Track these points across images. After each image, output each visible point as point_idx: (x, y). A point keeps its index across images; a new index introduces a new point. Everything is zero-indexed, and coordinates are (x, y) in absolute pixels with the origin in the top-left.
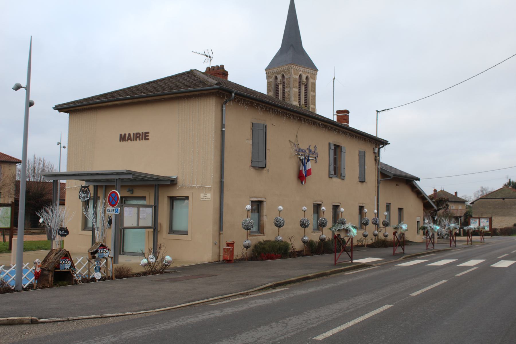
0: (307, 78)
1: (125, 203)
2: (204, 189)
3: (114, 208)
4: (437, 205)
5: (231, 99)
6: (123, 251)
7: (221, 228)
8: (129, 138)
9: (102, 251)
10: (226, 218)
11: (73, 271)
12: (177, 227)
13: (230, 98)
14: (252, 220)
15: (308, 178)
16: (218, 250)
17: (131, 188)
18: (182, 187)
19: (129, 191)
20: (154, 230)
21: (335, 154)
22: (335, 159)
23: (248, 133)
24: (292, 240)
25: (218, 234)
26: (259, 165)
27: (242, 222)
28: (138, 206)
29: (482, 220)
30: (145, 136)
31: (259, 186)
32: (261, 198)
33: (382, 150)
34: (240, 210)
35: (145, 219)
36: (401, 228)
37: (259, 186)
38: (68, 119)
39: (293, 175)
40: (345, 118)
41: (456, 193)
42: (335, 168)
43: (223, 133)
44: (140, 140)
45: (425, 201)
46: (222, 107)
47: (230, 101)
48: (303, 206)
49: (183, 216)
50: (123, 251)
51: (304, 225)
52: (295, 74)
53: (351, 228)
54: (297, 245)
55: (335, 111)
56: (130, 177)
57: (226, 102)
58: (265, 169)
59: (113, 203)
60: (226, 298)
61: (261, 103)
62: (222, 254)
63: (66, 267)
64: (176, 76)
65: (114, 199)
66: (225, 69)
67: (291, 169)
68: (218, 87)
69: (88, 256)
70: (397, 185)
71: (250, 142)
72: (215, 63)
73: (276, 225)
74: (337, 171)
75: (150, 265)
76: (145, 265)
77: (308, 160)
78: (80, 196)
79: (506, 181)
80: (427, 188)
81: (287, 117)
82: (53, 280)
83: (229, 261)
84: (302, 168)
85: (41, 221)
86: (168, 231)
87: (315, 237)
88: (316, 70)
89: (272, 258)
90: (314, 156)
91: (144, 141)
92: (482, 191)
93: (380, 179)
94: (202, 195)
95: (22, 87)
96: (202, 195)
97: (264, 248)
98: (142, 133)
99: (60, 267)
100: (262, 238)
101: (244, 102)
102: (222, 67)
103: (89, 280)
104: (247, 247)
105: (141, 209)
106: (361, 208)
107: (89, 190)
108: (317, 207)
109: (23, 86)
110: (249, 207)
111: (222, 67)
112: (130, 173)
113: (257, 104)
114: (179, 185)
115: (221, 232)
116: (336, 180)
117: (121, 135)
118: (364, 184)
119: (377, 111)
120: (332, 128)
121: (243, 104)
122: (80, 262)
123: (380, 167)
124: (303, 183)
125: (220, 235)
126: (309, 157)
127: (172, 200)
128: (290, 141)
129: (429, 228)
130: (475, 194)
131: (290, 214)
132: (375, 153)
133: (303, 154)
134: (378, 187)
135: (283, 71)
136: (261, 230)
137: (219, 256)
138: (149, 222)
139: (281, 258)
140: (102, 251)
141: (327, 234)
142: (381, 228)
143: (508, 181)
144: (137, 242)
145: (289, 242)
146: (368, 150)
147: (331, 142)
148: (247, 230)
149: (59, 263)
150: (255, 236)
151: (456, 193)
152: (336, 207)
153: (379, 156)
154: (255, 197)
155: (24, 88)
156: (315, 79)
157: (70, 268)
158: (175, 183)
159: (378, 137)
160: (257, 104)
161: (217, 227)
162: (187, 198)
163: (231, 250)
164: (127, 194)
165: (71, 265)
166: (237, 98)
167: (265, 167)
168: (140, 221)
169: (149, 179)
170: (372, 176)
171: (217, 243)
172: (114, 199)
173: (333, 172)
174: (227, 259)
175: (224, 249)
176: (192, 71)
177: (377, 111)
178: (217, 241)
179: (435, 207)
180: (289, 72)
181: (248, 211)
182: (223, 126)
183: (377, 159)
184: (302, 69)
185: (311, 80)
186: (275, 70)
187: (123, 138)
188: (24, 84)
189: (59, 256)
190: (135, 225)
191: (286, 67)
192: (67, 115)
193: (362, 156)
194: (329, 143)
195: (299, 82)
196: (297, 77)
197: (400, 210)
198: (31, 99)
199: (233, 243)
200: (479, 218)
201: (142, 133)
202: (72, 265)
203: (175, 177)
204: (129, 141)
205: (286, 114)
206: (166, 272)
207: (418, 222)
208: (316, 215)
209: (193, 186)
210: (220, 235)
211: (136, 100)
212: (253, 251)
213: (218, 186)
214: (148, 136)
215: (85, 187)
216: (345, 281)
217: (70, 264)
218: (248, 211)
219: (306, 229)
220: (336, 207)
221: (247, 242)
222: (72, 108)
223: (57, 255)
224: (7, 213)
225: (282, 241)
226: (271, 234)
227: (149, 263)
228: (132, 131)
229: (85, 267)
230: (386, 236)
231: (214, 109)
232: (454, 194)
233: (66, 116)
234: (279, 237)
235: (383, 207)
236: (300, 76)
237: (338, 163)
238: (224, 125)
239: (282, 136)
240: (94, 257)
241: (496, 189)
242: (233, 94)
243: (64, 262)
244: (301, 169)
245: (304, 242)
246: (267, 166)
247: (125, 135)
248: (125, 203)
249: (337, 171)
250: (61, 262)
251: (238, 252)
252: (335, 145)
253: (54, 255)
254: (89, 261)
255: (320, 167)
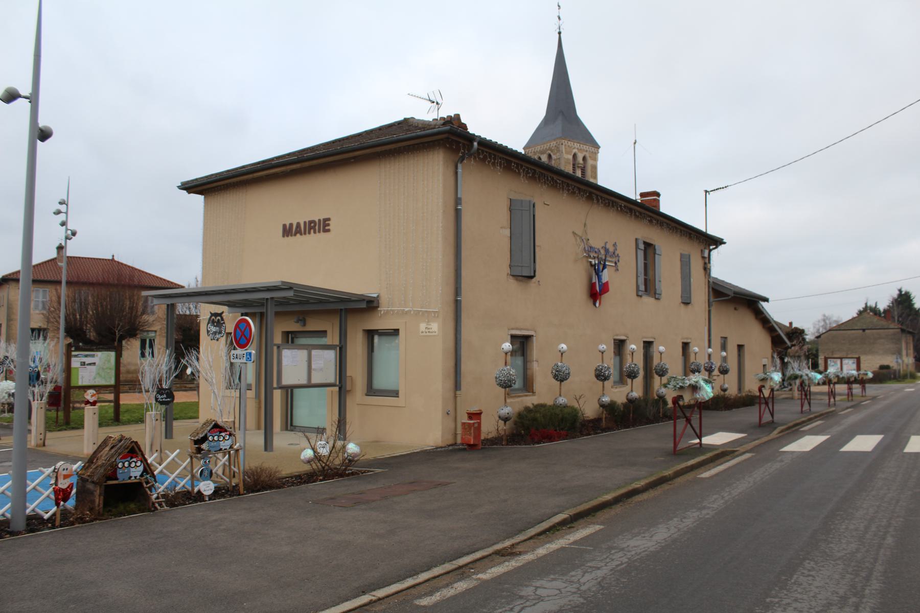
0: (584, 158)
1: (293, 342)
2: (428, 316)
3: (245, 352)
4: (785, 341)
5: (472, 151)
6: (291, 425)
7: (457, 386)
8: (298, 231)
9: (216, 438)
10: (467, 366)
11: (147, 483)
12: (380, 382)
13: (469, 150)
14: (513, 371)
15: (605, 297)
16: (452, 425)
17: (302, 317)
18: (387, 312)
19: (297, 322)
20: (340, 389)
21: (645, 259)
22: (646, 265)
23: (503, 216)
24: (581, 402)
25: (452, 394)
26: (524, 274)
27: (496, 373)
28: (310, 348)
29: (845, 361)
30: (323, 226)
31: (525, 309)
32: (528, 330)
33: (714, 254)
34: (490, 352)
35: (321, 369)
36: (771, 378)
37: (525, 309)
38: (202, 204)
39: (580, 290)
40: (654, 204)
41: (791, 324)
42: (646, 280)
43: (458, 213)
44: (315, 232)
45: (774, 335)
46: (456, 168)
47: (470, 156)
48: (601, 343)
49: (392, 362)
50: (291, 425)
51: (601, 376)
52: (567, 153)
53: (702, 383)
54: (590, 410)
55: (638, 194)
56: (290, 294)
57: (462, 159)
58: (534, 280)
59: (243, 341)
60: (461, 572)
61: (524, 164)
62: (459, 431)
63: (133, 474)
64: (380, 129)
65: (243, 334)
66: (463, 121)
67: (576, 280)
68: (447, 128)
69: (191, 448)
70: (735, 309)
71: (507, 232)
72: (446, 112)
73: (556, 377)
74: (648, 286)
75: (320, 460)
76: (309, 462)
77: (604, 267)
78: (208, 332)
79: (861, 307)
80: (779, 312)
81: (568, 190)
82: (101, 502)
83: (472, 447)
84: (595, 279)
85: (189, 371)
86: (365, 391)
87: (618, 394)
88: (597, 147)
89: (550, 438)
90: (614, 260)
91: (322, 234)
92: (824, 320)
93: (712, 299)
94: (423, 326)
95: (20, 96)
96: (423, 326)
97: (535, 419)
98: (319, 220)
99: (119, 476)
100: (530, 401)
101: (495, 159)
102: (457, 117)
103: (192, 497)
104: (505, 419)
105: (314, 352)
106: (685, 346)
107: (222, 319)
108: (620, 345)
109: (22, 94)
110: (507, 346)
111: (457, 117)
112: (290, 287)
113: (517, 164)
114: (383, 308)
115: (458, 392)
116: (648, 300)
117: (284, 226)
118: (690, 306)
119: (706, 191)
120: (640, 213)
121: (494, 164)
122: (173, 459)
123: (711, 280)
124: (597, 305)
125: (455, 397)
126: (605, 260)
127: (370, 334)
128: (574, 233)
129: (805, 377)
130: (814, 325)
131: (576, 360)
132: (704, 258)
133: (596, 255)
134: (709, 311)
135: (550, 149)
136: (528, 386)
137: (456, 435)
138: (331, 378)
139: (566, 437)
140: (216, 438)
141: (636, 389)
142: (715, 378)
143: (864, 306)
144: (315, 409)
145: (576, 405)
146: (693, 251)
147: (639, 237)
148: (505, 388)
149: (115, 468)
150: (519, 396)
151: (791, 324)
152: (648, 345)
153: (709, 262)
154: (517, 329)
155: (26, 98)
156: (595, 159)
157: (142, 475)
158: (375, 304)
159: (709, 232)
160: (517, 164)
161: (450, 384)
162: (396, 332)
163: (476, 425)
164: (294, 326)
165: (145, 470)
166: (483, 151)
167: (534, 276)
168: (313, 373)
169: (331, 300)
170: (700, 295)
171: (452, 413)
172: (243, 334)
173: (642, 288)
174: (470, 444)
175: (464, 424)
176: (406, 120)
177: (706, 191)
178: (451, 408)
179: (789, 343)
180: (558, 149)
181: (506, 354)
182: (458, 201)
183: (706, 269)
184: (577, 145)
185: (590, 162)
186: (538, 148)
187: (287, 231)
188: (25, 89)
189: (116, 451)
190: (304, 381)
191: (553, 144)
192: (201, 198)
193: (685, 262)
194: (636, 240)
195: (574, 165)
196: (571, 157)
197: (740, 347)
198: (42, 123)
199: (480, 414)
200: (841, 359)
201: (319, 220)
202: (148, 469)
203: (375, 295)
204: (298, 235)
205: (568, 185)
206: (352, 474)
207: (764, 366)
208: (618, 358)
209: (406, 309)
210: (455, 397)
211: (306, 164)
212: (515, 423)
213: (450, 309)
214: (329, 225)
215: (216, 315)
216: (715, 503)
217: (141, 468)
218: (506, 354)
219: (606, 382)
220: (648, 345)
221: (506, 411)
222: (206, 187)
223: (113, 450)
224: (109, 361)
225: (566, 406)
226: (545, 392)
227: (317, 457)
228: (301, 217)
229: (185, 468)
230: (725, 390)
231: (441, 163)
232: (788, 325)
233: (199, 199)
234: (560, 399)
235: (717, 342)
236: (575, 156)
237: (650, 273)
238: (460, 199)
239: (560, 224)
240: (199, 450)
241: (850, 318)
242: (475, 144)
243: (126, 464)
244: (594, 281)
245: (602, 406)
246: (537, 273)
247: (291, 225)
248: (293, 342)
249: (648, 286)
250: (120, 465)
251: (490, 427)
252: (645, 243)
253: (107, 449)
254: (191, 458)
255: (622, 279)
